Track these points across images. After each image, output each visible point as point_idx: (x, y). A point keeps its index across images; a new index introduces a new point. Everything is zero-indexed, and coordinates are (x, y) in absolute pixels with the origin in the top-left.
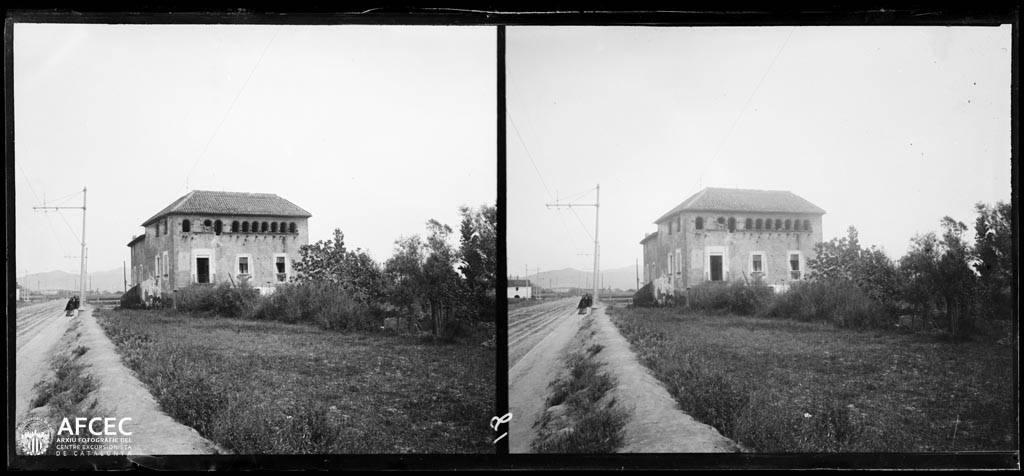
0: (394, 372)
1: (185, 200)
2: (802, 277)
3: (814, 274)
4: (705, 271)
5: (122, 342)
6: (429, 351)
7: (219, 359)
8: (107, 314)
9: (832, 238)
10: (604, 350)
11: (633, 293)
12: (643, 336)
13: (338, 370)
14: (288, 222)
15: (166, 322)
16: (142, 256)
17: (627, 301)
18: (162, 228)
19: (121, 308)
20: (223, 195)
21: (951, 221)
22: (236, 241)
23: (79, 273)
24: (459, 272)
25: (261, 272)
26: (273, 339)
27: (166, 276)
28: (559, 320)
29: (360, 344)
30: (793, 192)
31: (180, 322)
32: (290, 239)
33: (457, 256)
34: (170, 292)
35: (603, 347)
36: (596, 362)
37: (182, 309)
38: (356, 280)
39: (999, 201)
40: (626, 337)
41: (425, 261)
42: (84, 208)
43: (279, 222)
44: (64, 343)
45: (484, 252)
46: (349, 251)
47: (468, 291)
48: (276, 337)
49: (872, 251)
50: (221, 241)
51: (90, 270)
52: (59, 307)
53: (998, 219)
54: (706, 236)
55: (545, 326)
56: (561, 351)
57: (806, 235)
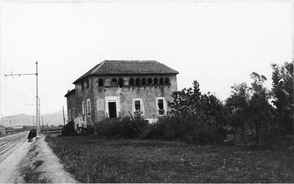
0: (234, 168)
1: (100, 66)
2: (165, 113)
3: (173, 111)
4: (106, 112)
5: (64, 156)
6: (255, 154)
7: (125, 164)
8: (53, 139)
9: (183, 89)
10: (43, 163)
11: (61, 128)
12: (67, 154)
13: (199, 169)
14: (164, 78)
15: (90, 143)
16: (74, 102)
17: (58, 132)
18: (85, 85)
19: (62, 135)
20: (123, 62)
21: (257, 75)
22: (133, 91)
23: (36, 115)
24: (272, 104)
25: (149, 110)
26: (158, 151)
27: (89, 114)
28: (16, 146)
29: (212, 152)
30: (158, 61)
31: (99, 142)
32: (166, 89)
33: (271, 94)
34: (92, 124)
35: (43, 162)
36: (39, 171)
37: (100, 135)
38: (208, 112)
39: (286, 61)
40: (57, 155)
41: (250, 98)
42: (37, 74)
43: (159, 78)
44: (28, 158)
45: (287, 92)
46: (203, 94)
47: (278, 116)
48: (160, 149)
49: (208, 95)
50: (123, 91)
51: (42, 113)
52: (24, 136)
53: (285, 73)
54: (105, 90)
55: (8, 150)
56: (18, 165)
57: (167, 87)
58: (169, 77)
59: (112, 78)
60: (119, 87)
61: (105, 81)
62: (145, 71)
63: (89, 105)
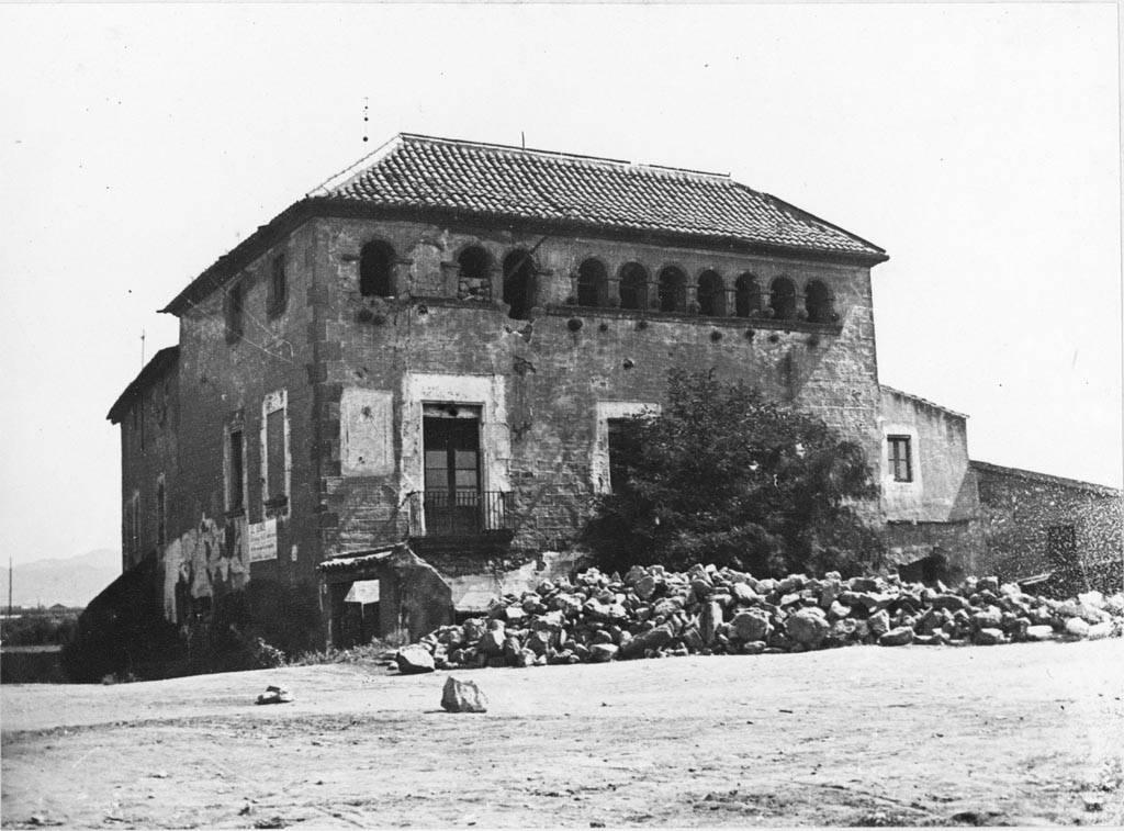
58: (827, 277)
59: (461, 239)
60: (505, 316)
61: (410, 256)
62: (693, 219)
63: (275, 441)
